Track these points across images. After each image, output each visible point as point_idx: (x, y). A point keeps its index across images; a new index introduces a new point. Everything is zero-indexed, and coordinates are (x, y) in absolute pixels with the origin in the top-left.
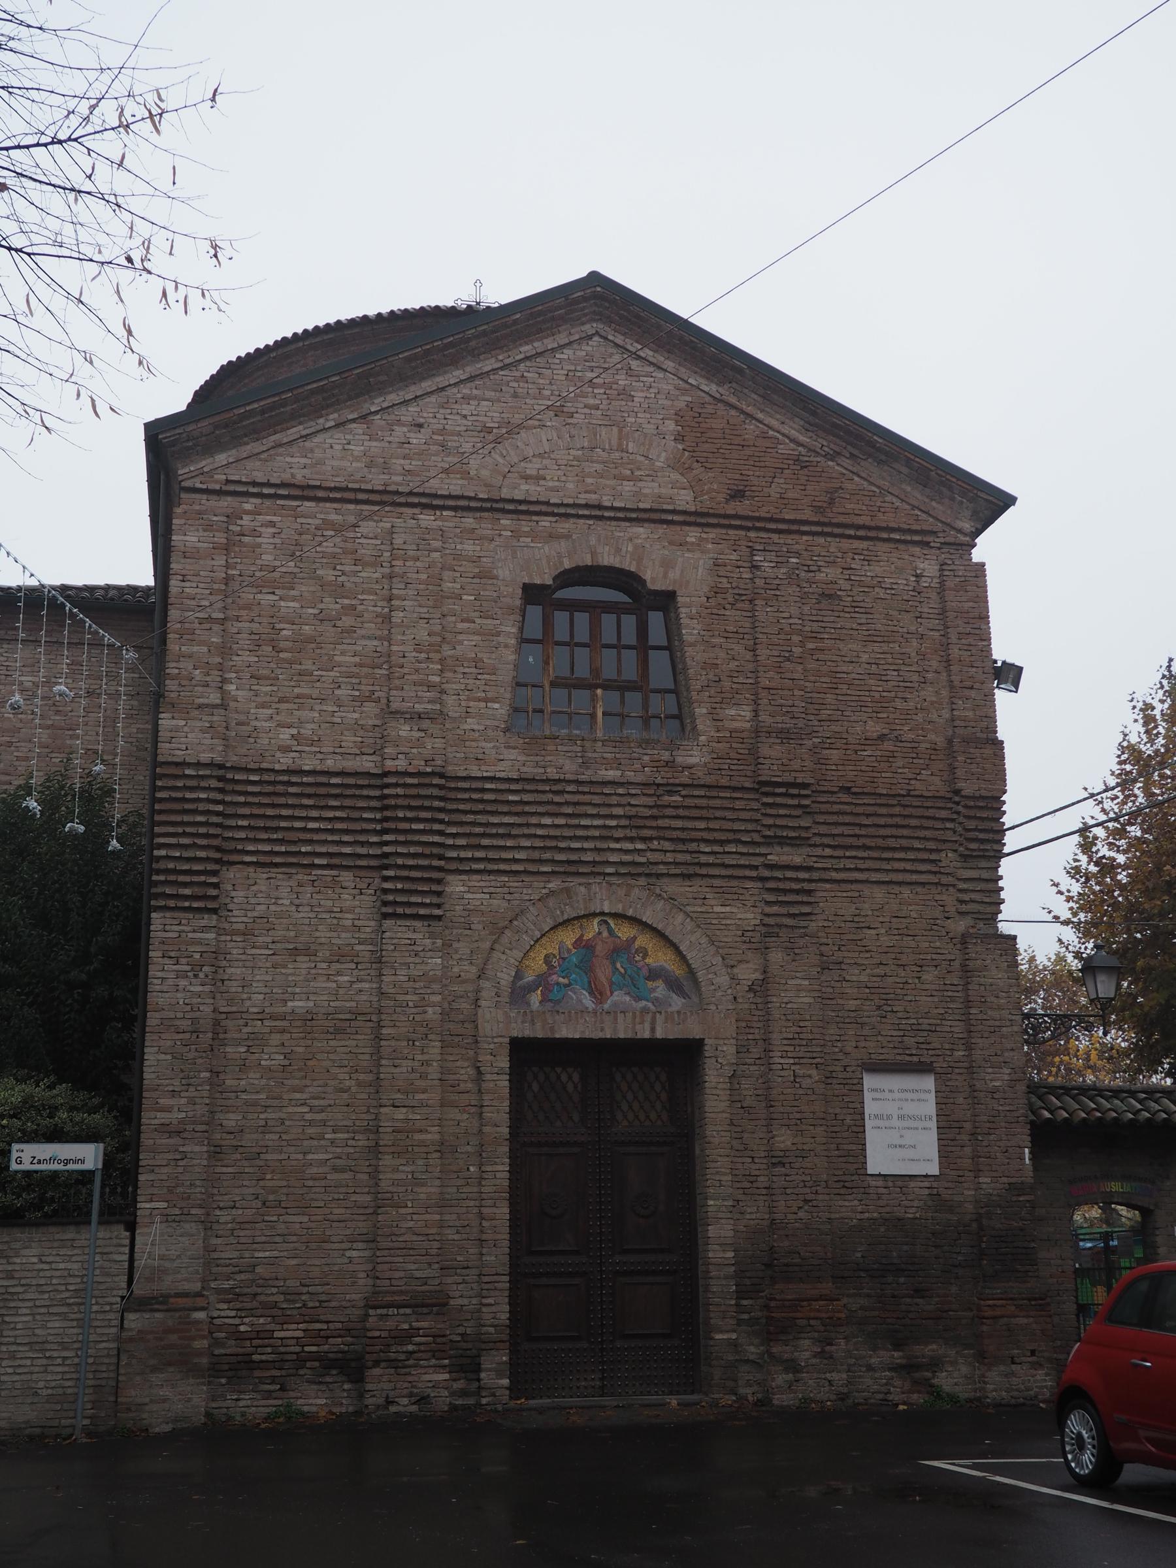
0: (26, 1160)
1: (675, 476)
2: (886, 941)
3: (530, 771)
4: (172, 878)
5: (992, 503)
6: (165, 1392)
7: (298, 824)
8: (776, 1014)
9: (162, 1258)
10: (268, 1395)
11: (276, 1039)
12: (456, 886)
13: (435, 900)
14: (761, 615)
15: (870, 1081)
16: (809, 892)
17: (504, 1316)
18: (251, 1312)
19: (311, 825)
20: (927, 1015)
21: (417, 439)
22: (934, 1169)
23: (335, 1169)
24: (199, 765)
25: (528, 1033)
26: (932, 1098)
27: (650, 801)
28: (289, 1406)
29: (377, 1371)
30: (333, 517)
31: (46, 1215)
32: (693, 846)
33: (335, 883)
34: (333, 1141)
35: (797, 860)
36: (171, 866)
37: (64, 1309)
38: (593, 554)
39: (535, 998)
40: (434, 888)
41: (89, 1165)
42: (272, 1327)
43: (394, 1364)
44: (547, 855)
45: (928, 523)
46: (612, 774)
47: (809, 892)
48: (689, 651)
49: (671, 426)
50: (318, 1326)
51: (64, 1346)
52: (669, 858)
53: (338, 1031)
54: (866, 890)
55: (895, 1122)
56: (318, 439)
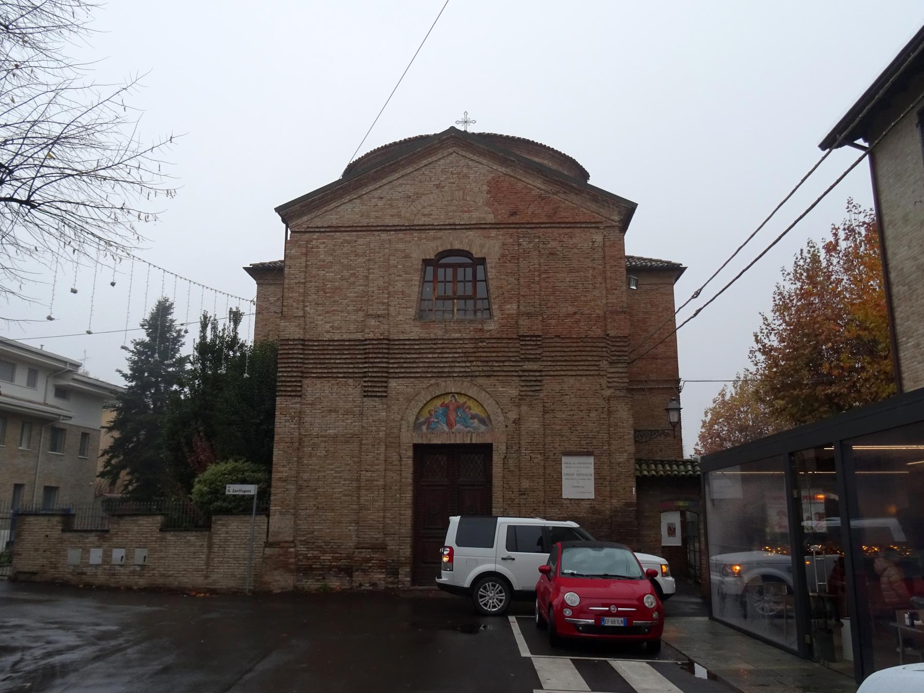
1: (486, 208)
2: (574, 400)
3: (423, 336)
10: (318, 581)
11: (323, 445)
12: (393, 383)
15: (565, 459)
18: (312, 549)
19: (338, 361)
21: (380, 204)
23: (345, 495)
25: (420, 442)
30: (347, 238)
33: (346, 384)
39: (424, 428)
41: (252, 493)
45: (599, 218)
46: (457, 335)
49: (485, 188)
53: (347, 442)
54: (566, 379)
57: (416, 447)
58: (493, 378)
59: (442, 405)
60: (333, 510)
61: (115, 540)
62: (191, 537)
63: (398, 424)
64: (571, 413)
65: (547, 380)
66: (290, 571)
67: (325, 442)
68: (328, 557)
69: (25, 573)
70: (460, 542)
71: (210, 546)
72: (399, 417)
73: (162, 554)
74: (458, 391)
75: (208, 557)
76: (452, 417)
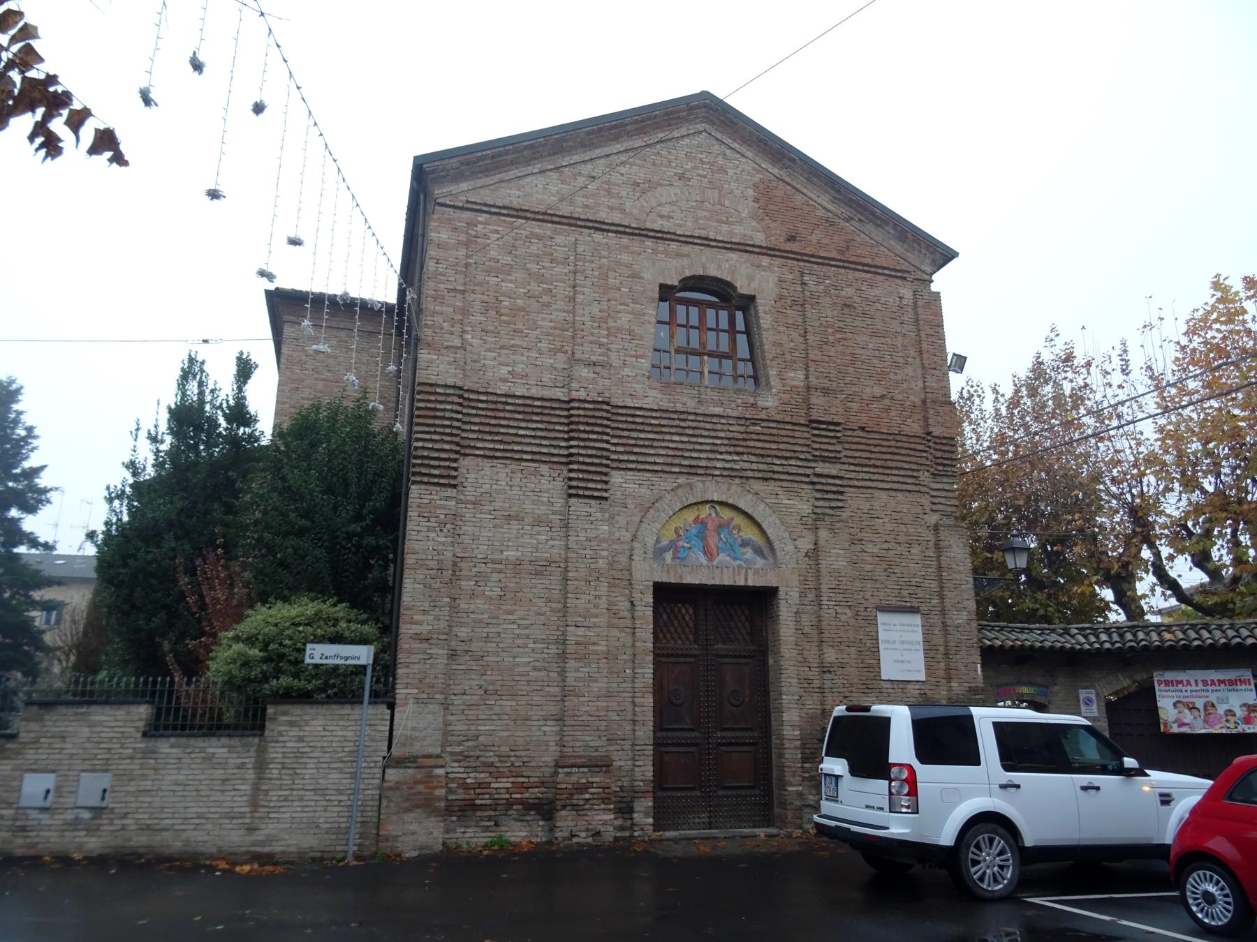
1: (754, 223)
2: (889, 526)
4: (426, 462)
5: (944, 255)
7: (512, 431)
8: (824, 572)
9: (413, 729)
10: (486, 829)
11: (495, 577)
12: (616, 478)
13: (604, 487)
14: (809, 315)
15: (882, 618)
16: (841, 493)
19: (521, 432)
23: (535, 669)
24: (446, 386)
26: (919, 630)
27: (742, 429)
28: (500, 837)
29: (564, 813)
30: (537, 231)
31: (328, 696)
32: (769, 460)
35: (834, 472)
36: (426, 453)
37: (341, 765)
38: (704, 268)
39: (668, 556)
40: (604, 478)
41: (362, 662)
43: (575, 807)
44: (677, 461)
45: (905, 266)
49: (750, 192)
51: (340, 792)
52: (754, 466)
53: (537, 573)
54: (877, 493)
55: (898, 646)
56: (529, 179)
58: (772, 483)
59: (696, 520)
60: (514, 695)
61: (31, 754)
62: (218, 748)
63: (627, 547)
64: (886, 546)
66: (435, 812)
67: (500, 572)
68: (505, 783)
71: (261, 766)
72: (629, 536)
73: (148, 784)
74: (723, 498)
75: (256, 789)
76: (712, 540)
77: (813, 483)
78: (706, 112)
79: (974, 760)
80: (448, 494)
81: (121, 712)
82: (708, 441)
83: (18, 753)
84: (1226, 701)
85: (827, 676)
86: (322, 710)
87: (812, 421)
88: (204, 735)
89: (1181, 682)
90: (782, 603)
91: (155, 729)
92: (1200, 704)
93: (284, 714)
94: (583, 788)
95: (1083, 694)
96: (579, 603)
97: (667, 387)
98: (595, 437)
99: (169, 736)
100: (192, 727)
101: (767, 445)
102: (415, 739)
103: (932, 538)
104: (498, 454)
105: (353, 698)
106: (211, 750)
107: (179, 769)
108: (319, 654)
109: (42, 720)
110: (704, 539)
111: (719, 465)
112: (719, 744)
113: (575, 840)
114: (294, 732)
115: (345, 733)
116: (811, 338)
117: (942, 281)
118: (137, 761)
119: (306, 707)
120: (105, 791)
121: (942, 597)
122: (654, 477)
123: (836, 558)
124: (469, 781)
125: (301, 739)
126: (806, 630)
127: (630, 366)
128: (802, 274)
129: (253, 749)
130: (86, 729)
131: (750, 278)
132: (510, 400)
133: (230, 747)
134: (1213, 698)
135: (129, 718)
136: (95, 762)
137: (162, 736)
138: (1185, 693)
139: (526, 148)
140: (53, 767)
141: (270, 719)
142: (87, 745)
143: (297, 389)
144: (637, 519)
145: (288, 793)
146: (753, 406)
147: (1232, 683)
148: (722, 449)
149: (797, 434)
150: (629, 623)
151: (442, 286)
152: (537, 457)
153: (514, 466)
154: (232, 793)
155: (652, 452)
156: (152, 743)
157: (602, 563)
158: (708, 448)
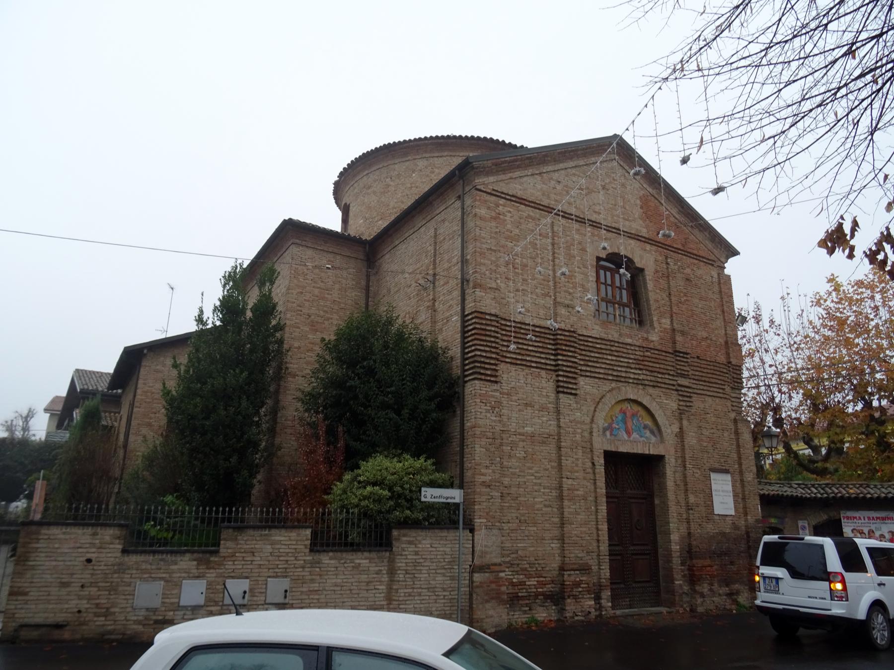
0: (429, 496)
1: (641, 222)
2: (713, 419)
3: (604, 336)
4: (483, 365)
5: (734, 252)
6: (491, 612)
7: (525, 347)
8: (686, 447)
9: (486, 546)
10: (525, 612)
11: (521, 444)
12: (582, 381)
13: (494, 373)
14: (671, 283)
15: (713, 476)
16: (690, 397)
17: (608, 574)
18: (517, 573)
19: (530, 348)
20: (726, 450)
21: (559, 187)
22: (733, 513)
23: (545, 506)
24: (490, 314)
25: (609, 449)
27: (641, 354)
28: (533, 617)
29: (569, 601)
30: (531, 214)
31: (430, 524)
32: (656, 374)
33: (539, 375)
34: (544, 493)
35: (687, 384)
36: (482, 360)
37: (443, 571)
38: (618, 248)
39: (608, 433)
40: (494, 367)
41: (457, 500)
42: (525, 580)
43: (575, 597)
44: (610, 372)
45: (713, 257)
46: (629, 341)
47: (690, 397)
48: (650, 294)
49: (638, 202)
50: (542, 579)
51: (444, 590)
52: (649, 378)
53: (544, 442)
54: (707, 398)
56: (525, 179)
57: (608, 455)
60: (535, 524)
61: (229, 565)
62: (362, 560)
64: (712, 431)
65: (695, 398)
66: (501, 602)
67: (523, 441)
68: (533, 582)
69: (38, 626)
70: (762, 564)
71: (392, 572)
73: (315, 586)
75: (390, 588)
76: (630, 424)
77: (677, 390)
78: (617, 150)
79: (864, 569)
80: (495, 388)
81: (293, 534)
82: (626, 360)
83: (220, 564)
84: (880, 529)
85: (691, 512)
86: (429, 533)
87: (676, 351)
88: (353, 551)
89: (855, 518)
90: (667, 465)
91: (319, 544)
92: (866, 531)
93: (405, 535)
94: (577, 584)
95: (800, 523)
96: (567, 462)
97: (605, 324)
98: (570, 354)
99: (328, 552)
100: (334, 545)
101: (655, 365)
102: (486, 553)
103: (733, 427)
104: (519, 362)
105: (453, 524)
106: (357, 561)
107: (336, 575)
108: (430, 495)
109: (236, 539)
110: (625, 423)
111: (632, 376)
112: (633, 554)
113: (576, 618)
114: (412, 548)
115: (445, 549)
116: (673, 298)
117: (731, 267)
118: (307, 569)
119: (419, 531)
120: (286, 591)
121: (740, 464)
122: (600, 382)
123: (691, 439)
124: (514, 580)
125: (417, 553)
126: (678, 483)
127: (583, 309)
128: (666, 258)
129: (385, 561)
130: (269, 547)
131: (641, 257)
132: (523, 326)
133: (370, 559)
134: (873, 527)
135: (299, 538)
136: (277, 570)
137: (324, 551)
138: (858, 524)
139: (527, 158)
140: (247, 575)
141: (396, 539)
142: (270, 558)
143: (302, 293)
144: (593, 409)
145: (411, 590)
146: (647, 339)
147: (883, 519)
148: (633, 366)
149: (668, 359)
150: (592, 476)
151: (484, 246)
152: (539, 365)
153: (527, 371)
154: (374, 591)
155: (598, 365)
156: (317, 557)
157: (578, 437)
158: (626, 365)
